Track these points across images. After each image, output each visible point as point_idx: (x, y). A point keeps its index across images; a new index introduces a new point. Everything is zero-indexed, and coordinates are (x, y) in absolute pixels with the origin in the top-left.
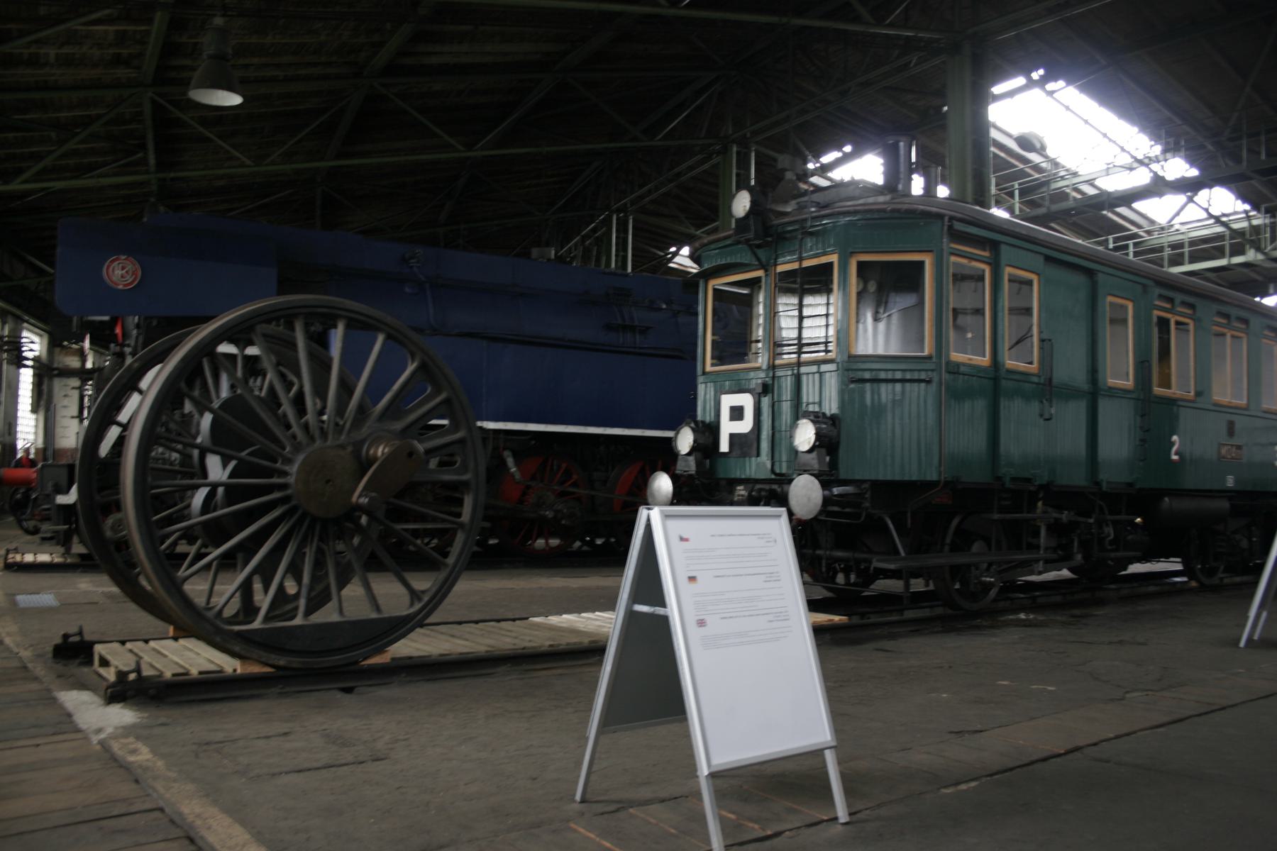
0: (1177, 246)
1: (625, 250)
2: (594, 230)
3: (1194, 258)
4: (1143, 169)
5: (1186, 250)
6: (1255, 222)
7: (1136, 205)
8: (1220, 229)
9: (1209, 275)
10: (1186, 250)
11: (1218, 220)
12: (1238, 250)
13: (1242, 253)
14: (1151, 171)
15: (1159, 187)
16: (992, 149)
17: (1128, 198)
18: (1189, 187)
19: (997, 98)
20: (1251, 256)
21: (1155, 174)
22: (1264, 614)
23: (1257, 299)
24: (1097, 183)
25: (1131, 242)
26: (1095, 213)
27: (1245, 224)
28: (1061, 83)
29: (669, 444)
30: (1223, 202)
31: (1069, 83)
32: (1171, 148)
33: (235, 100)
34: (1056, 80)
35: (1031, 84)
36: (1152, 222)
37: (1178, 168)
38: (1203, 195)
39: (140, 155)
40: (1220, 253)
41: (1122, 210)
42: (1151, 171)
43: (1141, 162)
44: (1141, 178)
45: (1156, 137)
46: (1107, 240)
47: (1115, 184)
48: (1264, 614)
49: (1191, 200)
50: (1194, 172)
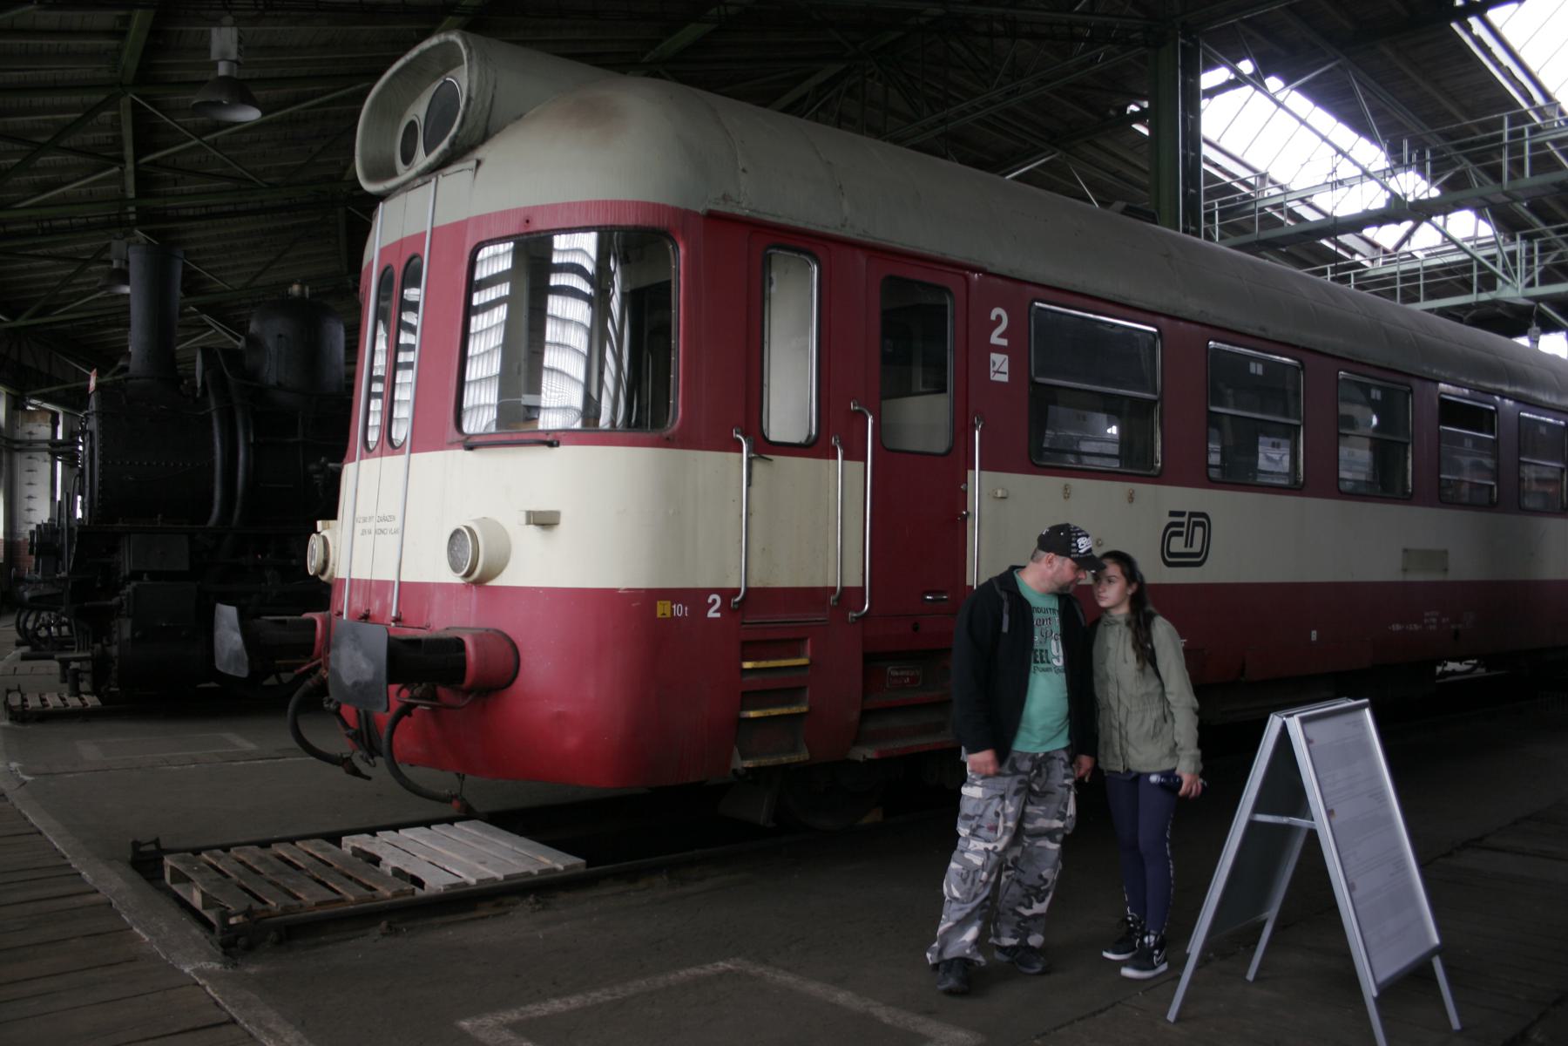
4: (1373, 186)
5: (1399, 286)
8: (1466, 257)
9: (194, 332)
10: (1399, 286)
16: (1204, 166)
17: (1356, 224)
18: (1420, 212)
21: (1394, 195)
23: (1524, 341)
24: (1317, 200)
25: (1352, 272)
26: (1309, 243)
29: (417, 284)
30: (1465, 225)
32: (1398, 163)
33: (1106, 954)
35: (1237, 82)
36: (1375, 246)
37: (1414, 185)
39: (116, 169)
40: (1467, 287)
41: (1348, 239)
43: (1366, 174)
44: (1374, 198)
47: (1346, 204)
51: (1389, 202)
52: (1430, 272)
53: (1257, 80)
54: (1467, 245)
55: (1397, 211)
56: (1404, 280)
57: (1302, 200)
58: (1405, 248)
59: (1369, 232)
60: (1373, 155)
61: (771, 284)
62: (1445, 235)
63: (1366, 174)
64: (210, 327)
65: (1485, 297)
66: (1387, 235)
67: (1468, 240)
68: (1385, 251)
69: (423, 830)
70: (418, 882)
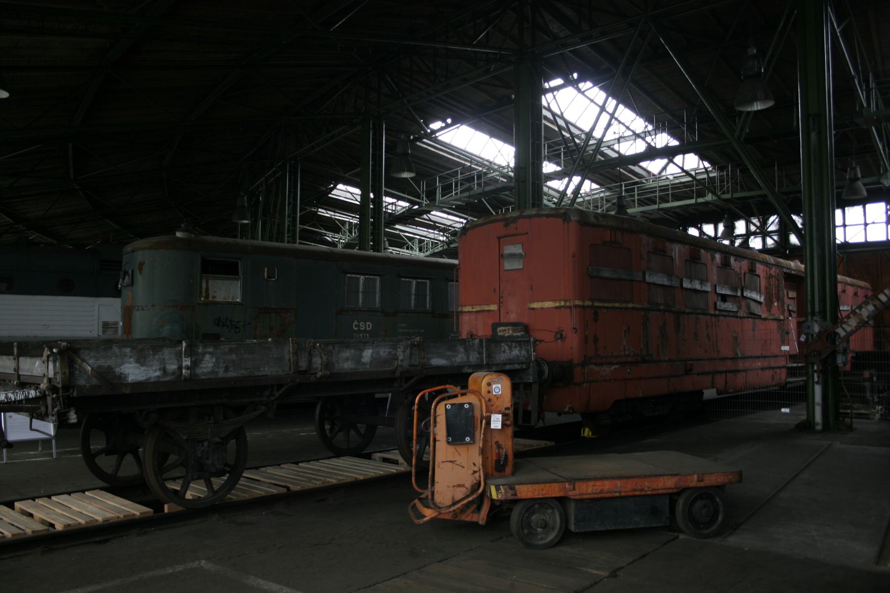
0: (664, 189)
1: (295, 199)
2: (275, 173)
3: (676, 198)
4: (639, 141)
6: (711, 175)
7: (642, 164)
8: (690, 179)
11: (687, 173)
12: (701, 194)
13: (703, 196)
14: (647, 142)
15: (652, 153)
16: (543, 121)
17: (637, 159)
18: (669, 153)
19: (547, 91)
20: (709, 197)
21: (649, 144)
22: (425, 140)
24: (616, 147)
27: (705, 176)
28: (589, 84)
30: (691, 161)
31: (595, 84)
32: (659, 127)
34: (585, 82)
36: (648, 172)
37: (663, 140)
38: (678, 159)
42: (647, 142)
44: (639, 147)
45: (649, 120)
46: (621, 186)
47: (631, 148)
48: (425, 140)
49: (671, 161)
50: (674, 143)
51: (647, 148)
52: (675, 187)
53: (575, 84)
54: (693, 173)
55: (652, 153)
56: (661, 191)
57: (609, 147)
58: (664, 174)
59: (644, 164)
60: (639, 124)
61: (560, 180)
62: (682, 168)
63: (637, 136)
64: (761, 188)
65: (700, 200)
66: (654, 166)
67: (692, 170)
68: (654, 175)
69: (65, 496)
70: (53, 526)
